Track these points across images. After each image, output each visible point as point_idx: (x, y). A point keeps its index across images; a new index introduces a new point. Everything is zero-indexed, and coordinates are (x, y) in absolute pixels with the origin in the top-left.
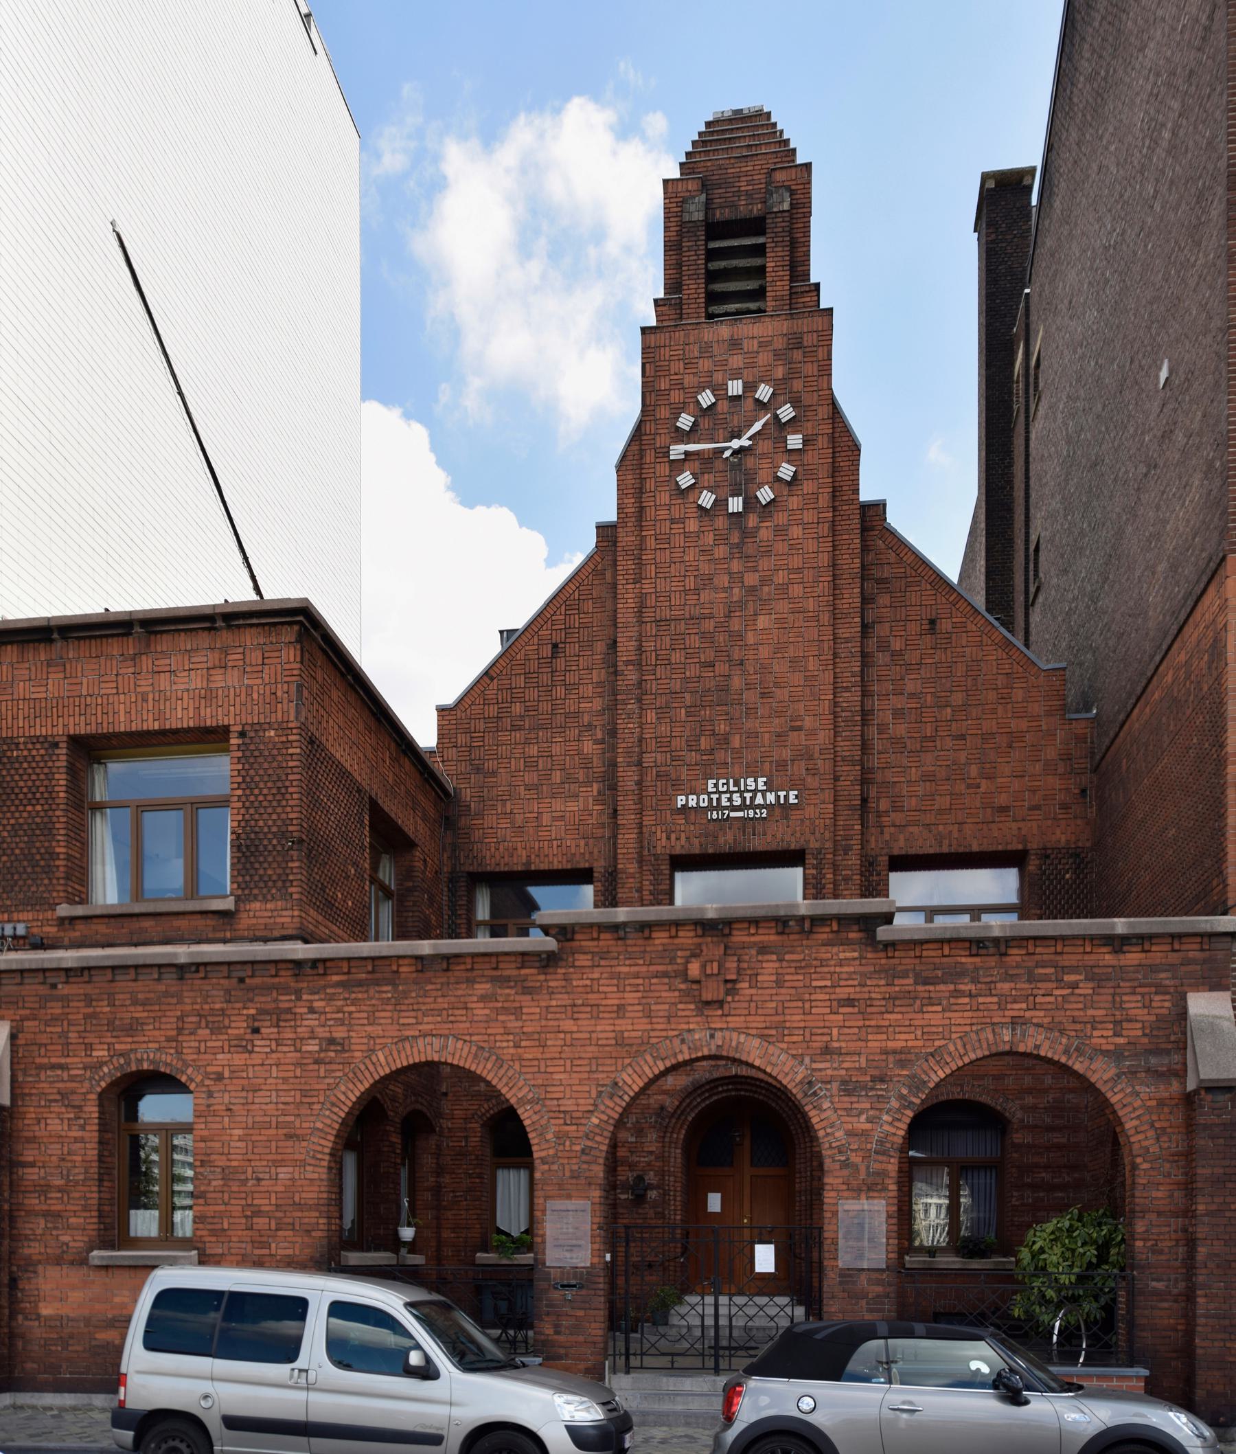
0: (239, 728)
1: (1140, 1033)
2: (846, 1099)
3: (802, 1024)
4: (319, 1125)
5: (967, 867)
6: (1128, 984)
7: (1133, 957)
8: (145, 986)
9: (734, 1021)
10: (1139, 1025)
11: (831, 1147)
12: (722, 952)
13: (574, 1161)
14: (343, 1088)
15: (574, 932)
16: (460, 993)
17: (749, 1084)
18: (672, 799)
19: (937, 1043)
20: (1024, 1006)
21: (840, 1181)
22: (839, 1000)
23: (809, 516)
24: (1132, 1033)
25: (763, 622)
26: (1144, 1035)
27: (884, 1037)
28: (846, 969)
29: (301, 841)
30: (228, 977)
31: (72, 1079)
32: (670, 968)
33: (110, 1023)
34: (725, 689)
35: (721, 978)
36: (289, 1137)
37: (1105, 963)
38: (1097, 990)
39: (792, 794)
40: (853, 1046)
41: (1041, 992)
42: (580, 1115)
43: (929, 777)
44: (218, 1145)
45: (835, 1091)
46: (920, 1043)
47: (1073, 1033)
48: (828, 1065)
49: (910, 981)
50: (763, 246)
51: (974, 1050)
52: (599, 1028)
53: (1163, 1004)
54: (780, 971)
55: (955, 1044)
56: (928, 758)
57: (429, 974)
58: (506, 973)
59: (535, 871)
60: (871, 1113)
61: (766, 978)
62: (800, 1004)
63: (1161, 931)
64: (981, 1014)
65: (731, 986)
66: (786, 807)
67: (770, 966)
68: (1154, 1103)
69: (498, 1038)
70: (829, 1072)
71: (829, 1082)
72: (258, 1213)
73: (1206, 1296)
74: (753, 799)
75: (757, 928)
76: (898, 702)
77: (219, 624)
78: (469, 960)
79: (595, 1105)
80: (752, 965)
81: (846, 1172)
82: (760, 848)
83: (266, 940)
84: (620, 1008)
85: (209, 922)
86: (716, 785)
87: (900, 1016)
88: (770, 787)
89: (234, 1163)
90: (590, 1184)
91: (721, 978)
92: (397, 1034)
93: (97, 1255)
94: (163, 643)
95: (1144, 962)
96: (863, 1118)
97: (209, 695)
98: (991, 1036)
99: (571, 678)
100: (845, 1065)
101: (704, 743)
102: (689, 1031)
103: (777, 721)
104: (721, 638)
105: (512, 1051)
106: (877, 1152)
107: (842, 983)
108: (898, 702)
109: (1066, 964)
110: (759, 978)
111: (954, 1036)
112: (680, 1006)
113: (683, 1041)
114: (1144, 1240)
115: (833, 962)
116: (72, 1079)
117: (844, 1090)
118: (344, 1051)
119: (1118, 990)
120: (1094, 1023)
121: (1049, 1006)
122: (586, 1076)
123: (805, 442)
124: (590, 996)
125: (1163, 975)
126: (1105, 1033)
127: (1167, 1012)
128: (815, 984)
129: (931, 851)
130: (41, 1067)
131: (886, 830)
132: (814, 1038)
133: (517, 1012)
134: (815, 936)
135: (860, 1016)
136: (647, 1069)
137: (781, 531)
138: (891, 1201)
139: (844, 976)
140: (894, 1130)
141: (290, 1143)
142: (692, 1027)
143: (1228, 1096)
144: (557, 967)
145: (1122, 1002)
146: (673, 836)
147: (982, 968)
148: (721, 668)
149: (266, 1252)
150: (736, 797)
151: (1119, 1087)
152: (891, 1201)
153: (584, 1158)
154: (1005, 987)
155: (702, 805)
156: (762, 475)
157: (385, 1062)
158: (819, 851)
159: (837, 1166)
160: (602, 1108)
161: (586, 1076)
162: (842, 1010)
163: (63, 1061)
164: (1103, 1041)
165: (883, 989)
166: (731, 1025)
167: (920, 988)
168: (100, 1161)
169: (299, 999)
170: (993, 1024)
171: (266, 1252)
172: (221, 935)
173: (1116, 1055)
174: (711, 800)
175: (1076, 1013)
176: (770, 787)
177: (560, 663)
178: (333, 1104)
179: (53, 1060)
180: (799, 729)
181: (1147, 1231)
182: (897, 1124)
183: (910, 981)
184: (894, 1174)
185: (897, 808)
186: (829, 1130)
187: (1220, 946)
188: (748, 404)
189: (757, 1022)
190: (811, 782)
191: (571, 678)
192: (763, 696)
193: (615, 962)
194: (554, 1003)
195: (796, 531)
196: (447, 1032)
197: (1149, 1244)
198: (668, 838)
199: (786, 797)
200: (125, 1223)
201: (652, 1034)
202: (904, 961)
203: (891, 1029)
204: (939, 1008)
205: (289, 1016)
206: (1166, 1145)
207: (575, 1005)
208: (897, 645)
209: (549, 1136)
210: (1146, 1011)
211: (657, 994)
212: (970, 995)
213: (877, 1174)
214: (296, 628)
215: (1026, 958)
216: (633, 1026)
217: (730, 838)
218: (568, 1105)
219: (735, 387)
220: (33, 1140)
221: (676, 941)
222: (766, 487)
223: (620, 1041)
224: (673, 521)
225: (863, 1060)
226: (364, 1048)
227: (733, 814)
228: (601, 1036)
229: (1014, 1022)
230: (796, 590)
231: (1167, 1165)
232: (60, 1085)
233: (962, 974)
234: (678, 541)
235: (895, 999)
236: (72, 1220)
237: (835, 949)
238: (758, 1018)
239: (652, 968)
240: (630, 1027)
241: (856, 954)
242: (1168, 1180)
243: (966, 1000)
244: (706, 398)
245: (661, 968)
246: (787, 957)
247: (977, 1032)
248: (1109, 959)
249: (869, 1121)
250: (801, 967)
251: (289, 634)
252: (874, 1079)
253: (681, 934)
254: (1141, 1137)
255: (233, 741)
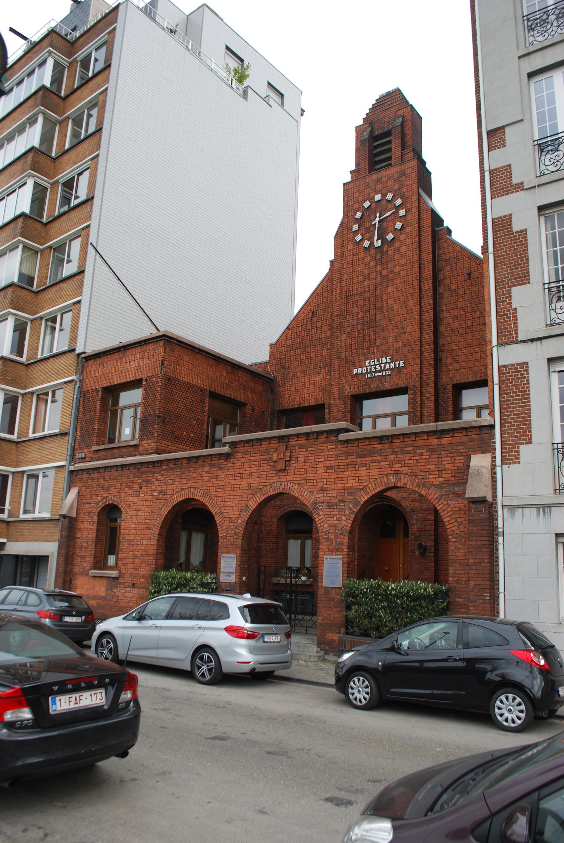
0: (145, 379)
1: (450, 475)
2: (329, 510)
3: (313, 478)
4: (156, 524)
5: (481, 387)
6: (444, 453)
7: (447, 440)
8: (113, 474)
9: (289, 478)
10: (450, 472)
11: (322, 532)
12: (285, 449)
13: (232, 538)
14: (163, 509)
15: (236, 445)
16: (200, 471)
17: (385, 498)
18: (352, 371)
19: (364, 484)
20: (400, 465)
21: (325, 547)
22: (327, 467)
23: (409, 241)
24: (446, 476)
25: (390, 289)
26: (452, 476)
27: (344, 482)
28: (330, 453)
29: (159, 417)
30: (135, 469)
31: (92, 507)
32: (268, 457)
33: (103, 486)
34: (375, 320)
35: (284, 460)
36: (147, 528)
37: (435, 443)
38: (431, 456)
39: (402, 362)
40: (332, 487)
41: (407, 458)
42: (234, 519)
43: (469, 345)
44: (127, 531)
45: (324, 507)
46: (358, 484)
47: (421, 477)
48: (322, 495)
49: (354, 457)
50: (390, 140)
51: (379, 487)
52: (243, 483)
53: (460, 461)
54: (306, 455)
55: (372, 485)
56: (470, 336)
57: (191, 464)
58: (215, 462)
59: (303, 407)
60: (338, 516)
61: (301, 459)
62: (313, 469)
63: (458, 427)
64: (382, 470)
65: (287, 463)
66: (399, 368)
67: (302, 454)
68: (457, 509)
69: (211, 488)
70: (323, 498)
71: (323, 503)
72: (136, 557)
73: (473, 606)
74: (385, 367)
75: (298, 438)
76: (454, 313)
77: (143, 344)
78: (202, 458)
79: (240, 515)
80: (296, 454)
81: (327, 543)
82: (388, 388)
83: (146, 454)
84: (250, 474)
85: (132, 449)
86: (369, 363)
87: (350, 473)
88: (392, 360)
89: (131, 538)
90: (236, 548)
91: (284, 460)
92: (180, 488)
93: (92, 572)
94: (129, 352)
95: (451, 442)
96: (335, 518)
97: (138, 368)
98: (386, 480)
99: (319, 324)
100: (329, 495)
101: (365, 345)
102: (274, 482)
103: (395, 331)
104: (372, 299)
105: (214, 493)
106: (340, 534)
107: (329, 459)
108: (454, 313)
109: (418, 445)
110: (299, 459)
111: (371, 480)
112: (270, 472)
113: (271, 487)
114: (453, 577)
115: (325, 451)
116: (92, 507)
117: (328, 506)
118: (164, 495)
119: (440, 456)
120: (430, 472)
121: (410, 465)
122: (237, 502)
123: (406, 212)
124: (241, 470)
125: (460, 448)
126: (435, 476)
127: (461, 464)
128: (319, 460)
129: (472, 380)
130: (85, 503)
131: (450, 372)
132: (318, 484)
133: (217, 477)
134: (319, 440)
135: (335, 473)
136: (258, 499)
137: (397, 250)
138: (345, 556)
139: (329, 456)
140: (346, 524)
141: (147, 531)
142: (274, 481)
143: (482, 505)
144: (231, 459)
145: (442, 461)
146: (352, 387)
147: (383, 449)
148: (373, 312)
149: (137, 572)
150: (378, 367)
151: (441, 502)
152: (345, 556)
153: (235, 537)
154: (392, 457)
155: (364, 372)
156: (390, 229)
157: (177, 499)
158: (414, 386)
159: (324, 540)
160: (242, 516)
161: (237, 502)
162: (328, 471)
163: (90, 501)
164: (434, 480)
165: (344, 461)
166: (288, 480)
167: (358, 460)
168: (96, 537)
169: (154, 476)
170: (387, 474)
171: (137, 572)
172: (134, 453)
173: (439, 486)
174: (367, 369)
175: (422, 467)
176: (392, 360)
177: (315, 319)
178: (160, 515)
179: (88, 501)
180: (405, 333)
181: (454, 573)
182: (348, 521)
183: (354, 457)
184: (346, 544)
185: (455, 362)
186: (322, 524)
187: (485, 432)
188: (384, 202)
189: (297, 478)
190: (410, 355)
191: (319, 324)
192: (389, 320)
193: (249, 455)
194: (229, 473)
195: (403, 249)
196: (195, 486)
197: (455, 579)
198: (350, 388)
199: (399, 364)
200: (106, 560)
201: (261, 484)
202: (352, 448)
203: (346, 478)
204: (365, 468)
205: (150, 482)
206: (463, 530)
207: (235, 474)
208: (453, 287)
209: (224, 528)
210: (453, 465)
211: (262, 468)
212: (378, 462)
213: (340, 544)
214: (163, 341)
215: (401, 443)
216: (254, 482)
217: (375, 385)
218: (231, 515)
219: (378, 197)
220: (80, 529)
221: (271, 445)
222: (390, 234)
223: (249, 488)
224: (354, 255)
225: (336, 492)
226: (170, 493)
227: (376, 375)
228: (243, 486)
229: (396, 473)
230: (403, 273)
231: (464, 540)
232: (88, 510)
233: (375, 453)
234: (356, 263)
235: (348, 465)
236: (87, 559)
237: (326, 445)
238: (297, 476)
239: (262, 457)
240: (253, 482)
241: (334, 446)
242: (464, 547)
243: (376, 464)
244: (367, 204)
245: (265, 457)
246: (309, 449)
247: (380, 478)
248: (436, 441)
249: (337, 520)
250: (314, 453)
251: (161, 343)
252: (340, 501)
253: (272, 442)
254: (451, 526)
255: (144, 383)
